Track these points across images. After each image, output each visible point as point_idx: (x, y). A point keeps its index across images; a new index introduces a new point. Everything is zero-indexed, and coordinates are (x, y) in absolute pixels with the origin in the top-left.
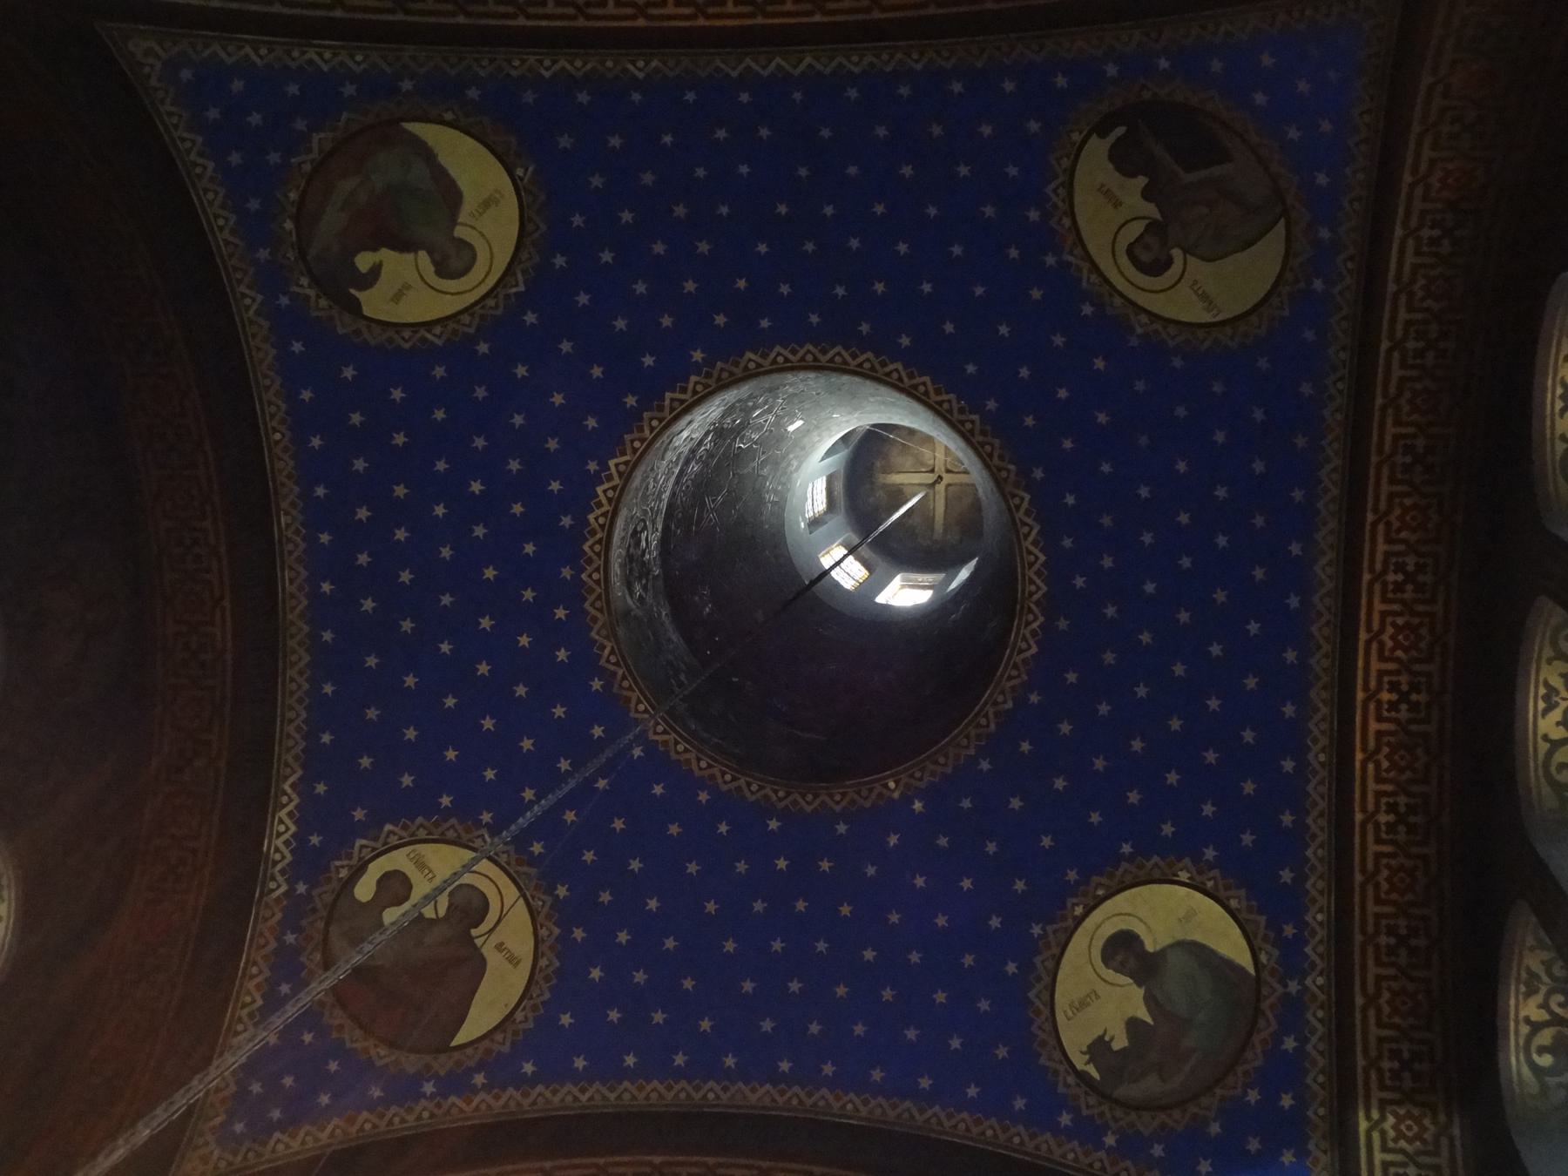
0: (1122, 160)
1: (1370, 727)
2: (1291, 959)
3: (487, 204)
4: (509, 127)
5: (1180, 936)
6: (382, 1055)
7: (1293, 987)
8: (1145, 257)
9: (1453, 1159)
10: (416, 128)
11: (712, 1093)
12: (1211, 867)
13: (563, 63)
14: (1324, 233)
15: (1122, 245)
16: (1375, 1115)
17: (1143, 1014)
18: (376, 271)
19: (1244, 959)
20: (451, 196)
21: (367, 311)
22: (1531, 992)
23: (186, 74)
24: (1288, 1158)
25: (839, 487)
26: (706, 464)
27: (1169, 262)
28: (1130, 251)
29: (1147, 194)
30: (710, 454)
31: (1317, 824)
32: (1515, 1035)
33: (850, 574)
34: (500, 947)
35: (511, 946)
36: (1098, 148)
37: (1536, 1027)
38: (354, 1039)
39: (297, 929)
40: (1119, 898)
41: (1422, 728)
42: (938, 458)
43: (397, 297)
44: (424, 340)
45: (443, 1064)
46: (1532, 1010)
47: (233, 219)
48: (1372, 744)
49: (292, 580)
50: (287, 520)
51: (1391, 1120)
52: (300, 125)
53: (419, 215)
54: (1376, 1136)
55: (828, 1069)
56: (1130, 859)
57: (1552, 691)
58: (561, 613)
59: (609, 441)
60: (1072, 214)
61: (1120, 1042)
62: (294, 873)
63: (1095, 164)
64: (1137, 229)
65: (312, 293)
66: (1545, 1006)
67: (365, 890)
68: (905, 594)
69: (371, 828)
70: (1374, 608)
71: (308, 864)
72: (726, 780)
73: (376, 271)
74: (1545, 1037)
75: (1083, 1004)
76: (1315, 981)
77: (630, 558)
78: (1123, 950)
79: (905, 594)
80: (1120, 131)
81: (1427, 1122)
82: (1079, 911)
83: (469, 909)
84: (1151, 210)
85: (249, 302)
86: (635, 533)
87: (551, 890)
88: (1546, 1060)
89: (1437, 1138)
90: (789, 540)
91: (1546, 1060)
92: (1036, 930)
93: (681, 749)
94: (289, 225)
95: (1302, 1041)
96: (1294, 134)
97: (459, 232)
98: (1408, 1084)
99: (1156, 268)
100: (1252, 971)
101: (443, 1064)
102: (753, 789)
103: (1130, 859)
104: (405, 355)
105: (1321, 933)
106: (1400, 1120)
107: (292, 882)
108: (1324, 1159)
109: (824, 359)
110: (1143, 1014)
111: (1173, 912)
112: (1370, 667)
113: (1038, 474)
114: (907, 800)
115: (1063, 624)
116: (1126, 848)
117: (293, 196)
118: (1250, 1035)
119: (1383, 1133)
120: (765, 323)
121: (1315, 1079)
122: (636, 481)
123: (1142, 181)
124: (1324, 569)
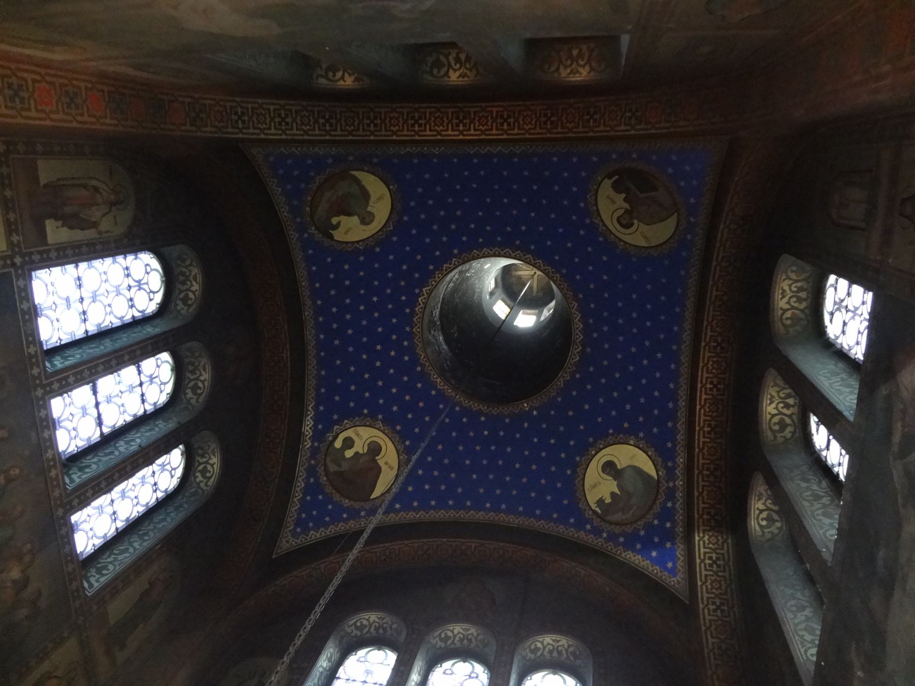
0: (617, 187)
1: (702, 397)
2: (670, 474)
3: (380, 199)
4: (388, 171)
5: (630, 464)
6: (346, 503)
7: (671, 484)
8: (624, 222)
9: (728, 552)
10: (353, 173)
11: (462, 515)
12: (641, 439)
13: (408, 149)
14: (692, 220)
15: (616, 215)
16: (701, 535)
17: (617, 491)
18: (339, 224)
19: (653, 473)
20: (366, 195)
21: (335, 238)
22: (759, 499)
23: (272, 159)
24: (668, 545)
25: (499, 279)
26: (455, 283)
27: (632, 224)
28: (619, 221)
29: (625, 200)
30: (457, 279)
31: (681, 426)
32: (753, 513)
33: (501, 309)
34: (386, 463)
35: (389, 457)
36: (607, 183)
37: (761, 511)
38: (329, 489)
39: (315, 459)
40: (607, 449)
41: (722, 397)
42: (530, 275)
43: (346, 233)
44: (356, 248)
45: (368, 505)
46: (760, 505)
47: (287, 208)
48: (703, 403)
49: (310, 334)
50: (308, 313)
51: (706, 537)
52: (312, 174)
53: (355, 204)
54: (701, 543)
55: (503, 506)
56: (612, 435)
57: (772, 397)
58: (406, 343)
59: (422, 283)
60: (597, 205)
61: (608, 500)
62: (314, 438)
63: (606, 189)
64: (621, 212)
65: (316, 232)
66: (764, 504)
67: (338, 444)
68: (526, 321)
69: (339, 422)
70: (705, 355)
71: (318, 436)
72: (466, 403)
73: (339, 224)
74: (764, 515)
75: (594, 486)
76: (679, 483)
77: (430, 321)
78: (609, 467)
79: (526, 321)
80: (617, 177)
81: (720, 538)
82: (593, 452)
83: (375, 449)
84: (627, 206)
85: (293, 236)
86: (432, 312)
87: (403, 443)
88: (764, 523)
89: (723, 543)
90: (485, 307)
91: (764, 523)
92: (578, 459)
93: (449, 392)
94: (308, 209)
95: (674, 504)
96: (682, 184)
97: (369, 209)
98: (713, 524)
99: (628, 226)
100: (656, 477)
101: (368, 505)
102: (475, 406)
103: (612, 435)
104: (350, 252)
105: (682, 466)
106: (710, 537)
107: (312, 442)
108: (682, 547)
109: (502, 253)
110: (617, 491)
111: (630, 455)
112: (703, 375)
113: (581, 296)
114: (531, 410)
115: (589, 350)
116: (611, 431)
117: (309, 198)
118: (655, 500)
119: (704, 542)
120: (481, 240)
121: (679, 517)
122: (433, 295)
123: (624, 195)
124: (687, 336)
